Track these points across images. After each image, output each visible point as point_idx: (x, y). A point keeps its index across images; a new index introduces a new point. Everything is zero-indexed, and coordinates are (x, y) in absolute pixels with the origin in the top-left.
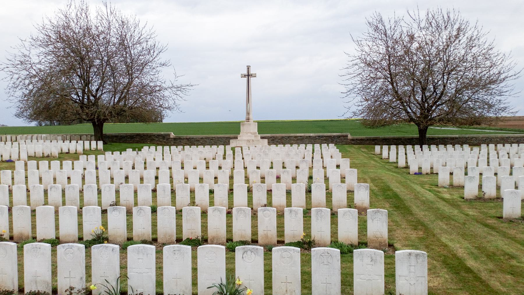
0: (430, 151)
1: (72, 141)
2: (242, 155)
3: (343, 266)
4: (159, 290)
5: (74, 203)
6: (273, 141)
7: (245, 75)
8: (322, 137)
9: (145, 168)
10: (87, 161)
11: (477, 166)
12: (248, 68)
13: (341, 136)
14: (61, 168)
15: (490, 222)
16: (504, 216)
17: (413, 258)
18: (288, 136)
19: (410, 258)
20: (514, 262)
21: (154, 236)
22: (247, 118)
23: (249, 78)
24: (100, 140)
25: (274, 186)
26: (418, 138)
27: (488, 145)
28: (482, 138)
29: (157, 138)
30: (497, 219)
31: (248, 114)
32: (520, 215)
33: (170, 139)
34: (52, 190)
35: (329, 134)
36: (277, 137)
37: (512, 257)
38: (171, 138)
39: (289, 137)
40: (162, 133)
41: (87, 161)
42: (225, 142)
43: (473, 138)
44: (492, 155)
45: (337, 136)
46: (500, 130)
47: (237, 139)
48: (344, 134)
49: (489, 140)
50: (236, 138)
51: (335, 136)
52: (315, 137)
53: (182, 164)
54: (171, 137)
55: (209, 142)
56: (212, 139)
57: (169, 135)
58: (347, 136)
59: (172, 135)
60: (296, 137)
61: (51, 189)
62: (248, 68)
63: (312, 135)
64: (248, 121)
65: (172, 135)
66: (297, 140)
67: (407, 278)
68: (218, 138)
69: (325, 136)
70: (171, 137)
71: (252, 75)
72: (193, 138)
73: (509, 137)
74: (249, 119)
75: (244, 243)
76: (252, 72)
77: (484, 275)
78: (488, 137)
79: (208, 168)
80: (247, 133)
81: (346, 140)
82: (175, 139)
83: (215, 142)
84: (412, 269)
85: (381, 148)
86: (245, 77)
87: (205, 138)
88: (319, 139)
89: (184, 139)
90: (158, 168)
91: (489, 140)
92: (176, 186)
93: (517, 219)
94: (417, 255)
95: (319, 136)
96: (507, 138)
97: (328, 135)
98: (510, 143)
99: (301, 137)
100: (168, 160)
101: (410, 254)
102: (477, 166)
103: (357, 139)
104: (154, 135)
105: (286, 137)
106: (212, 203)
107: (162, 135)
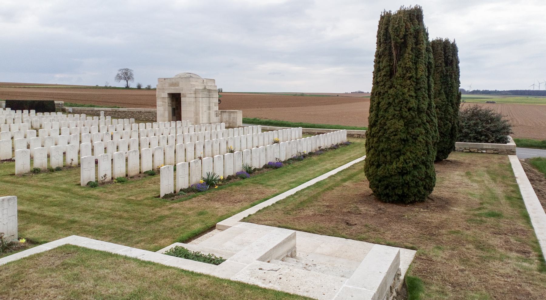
17: (6, 203)
32: (29, 170)
37: (47, 197)
93: (26, 173)
94: (9, 200)
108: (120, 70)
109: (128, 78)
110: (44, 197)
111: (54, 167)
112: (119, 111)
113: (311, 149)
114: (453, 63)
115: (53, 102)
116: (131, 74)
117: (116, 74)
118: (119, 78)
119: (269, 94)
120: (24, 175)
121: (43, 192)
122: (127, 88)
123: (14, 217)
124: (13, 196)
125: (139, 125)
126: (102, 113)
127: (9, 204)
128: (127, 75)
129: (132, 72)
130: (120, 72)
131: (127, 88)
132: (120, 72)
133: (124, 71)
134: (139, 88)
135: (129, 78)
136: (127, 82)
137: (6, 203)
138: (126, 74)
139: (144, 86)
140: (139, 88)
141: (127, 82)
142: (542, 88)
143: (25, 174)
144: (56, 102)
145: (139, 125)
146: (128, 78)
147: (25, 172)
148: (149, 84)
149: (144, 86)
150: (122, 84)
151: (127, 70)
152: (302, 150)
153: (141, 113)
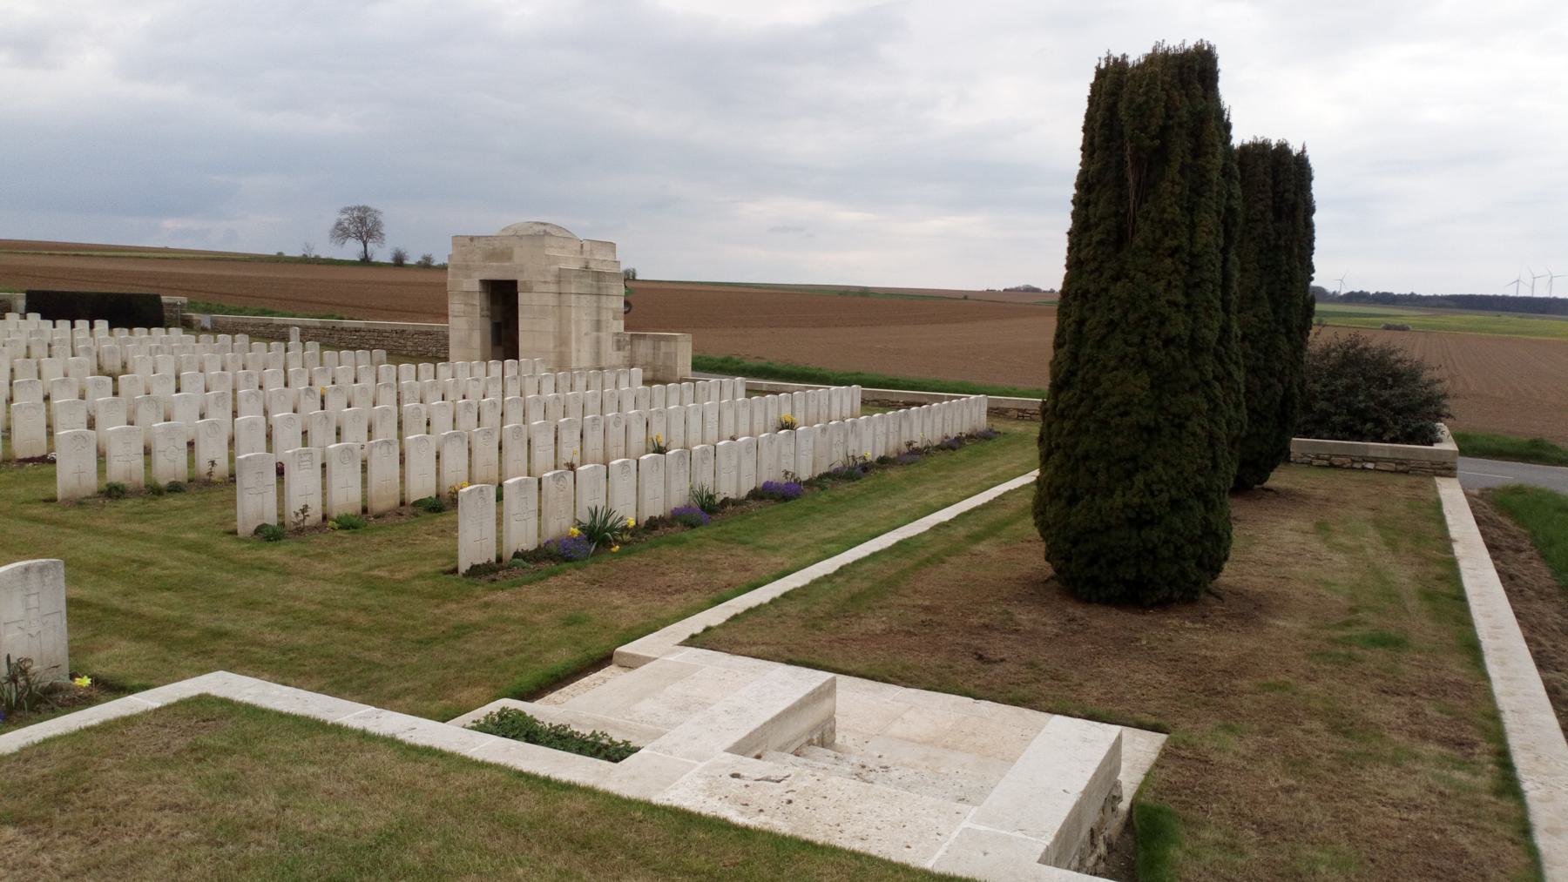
3: (233, 511)
11: (39, 377)
15: (35, 511)
16: (60, 497)
17: (33, 577)
19: (27, 578)
20: (155, 571)
24: (79, 318)
26: (1320, 426)
30: (45, 504)
32: (95, 489)
37: (145, 564)
61: (383, 417)
67: (23, 625)
77: (116, 602)
84: (33, 601)
93: (87, 498)
94: (42, 569)
98: (368, 349)
101: (27, 569)
102: (39, 377)
108: (344, 211)
109: (367, 233)
111: (163, 482)
112: (342, 329)
115: (157, 298)
116: (377, 223)
117: (334, 222)
118: (341, 232)
120: (80, 503)
122: (365, 261)
126: (295, 333)
128: (363, 225)
129: (380, 218)
130: (346, 216)
131: (365, 261)
132: (346, 216)
133: (356, 214)
134: (399, 262)
135: (370, 234)
136: (365, 246)
137: (34, 578)
138: (362, 221)
139: (412, 259)
140: (399, 262)
141: (365, 246)
144: (165, 299)
146: (367, 233)
148: (427, 253)
149: (412, 259)
150: (351, 250)
151: (365, 209)
153: (405, 336)
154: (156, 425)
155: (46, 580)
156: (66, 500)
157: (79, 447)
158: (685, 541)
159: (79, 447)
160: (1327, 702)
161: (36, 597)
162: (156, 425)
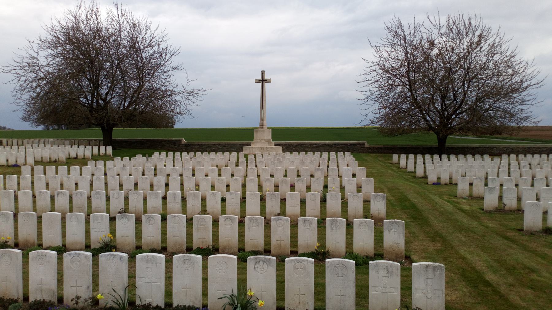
0: (458, 160)
1: (80, 146)
2: (256, 162)
4: (281, 304)
5: (81, 210)
6: (288, 148)
7: (259, 81)
8: (338, 144)
9: (155, 175)
10: (96, 166)
12: (263, 73)
13: (358, 144)
14: (69, 174)
15: (510, 234)
16: (525, 229)
17: (430, 271)
18: (303, 143)
19: (427, 270)
20: (534, 276)
21: (164, 245)
22: (261, 125)
23: (264, 83)
25: (288, 194)
27: (509, 156)
28: (503, 148)
29: (168, 144)
31: (262, 120)
32: (541, 228)
33: (182, 145)
34: (59, 196)
35: (345, 142)
36: (292, 144)
37: (532, 271)
38: (182, 144)
39: (304, 144)
40: (173, 139)
41: (96, 166)
42: (238, 149)
43: (494, 148)
44: (513, 166)
45: (354, 144)
46: (521, 140)
47: (251, 146)
48: (361, 142)
49: (510, 150)
50: (250, 145)
51: (351, 144)
52: (331, 145)
53: (194, 171)
54: (183, 143)
55: (221, 149)
56: (225, 145)
57: (180, 141)
58: (364, 144)
59: (184, 141)
60: (311, 145)
61: (58, 195)
62: (263, 73)
63: (327, 142)
64: (262, 128)
65: (184, 141)
66: (313, 147)
67: (424, 291)
68: (231, 144)
69: (341, 144)
70: (183, 143)
71: (266, 80)
72: (205, 145)
73: (531, 147)
74: (262, 126)
75: (256, 253)
76: (266, 77)
77: (503, 289)
78: (509, 147)
79: (220, 175)
80: (261, 140)
81: (363, 148)
82: (186, 145)
83: (227, 149)
84: (429, 282)
85: (399, 157)
86: (259, 82)
87: (217, 145)
88: (335, 147)
89: (195, 145)
90: (168, 175)
91: (510, 150)
92: (187, 193)
93: (537, 231)
94: (434, 268)
95: (335, 144)
96: (529, 148)
97: (344, 143)
99: (316, 144)
100: (178, 167)
101: (427, 266)
103: (374, 148)
104: (165, 141)
105: (301, 144)
106: (223, 212)
107: (173, 141)
110: (529, 270)
113: (532, 173)
114: (200, 144)
119: (125, 295)
120: (532, 233)
121: (531, 263)
123: (441, 292)
124: (441, 265)
125: (205, 267)
127: (435, 274)
137: (430, 271)
142: (329, 304)
143: (534, 233)
145: (205, 267)
147: (535, 230)
152: (42, 297)
154: (85, 191)
155: (436, 273)
156: (527, 231)
157: (535, 209)
158: (493, 46)
159: (535, 209)
160: (147, 30)
161: (431, 280)
162: (85, 191)
